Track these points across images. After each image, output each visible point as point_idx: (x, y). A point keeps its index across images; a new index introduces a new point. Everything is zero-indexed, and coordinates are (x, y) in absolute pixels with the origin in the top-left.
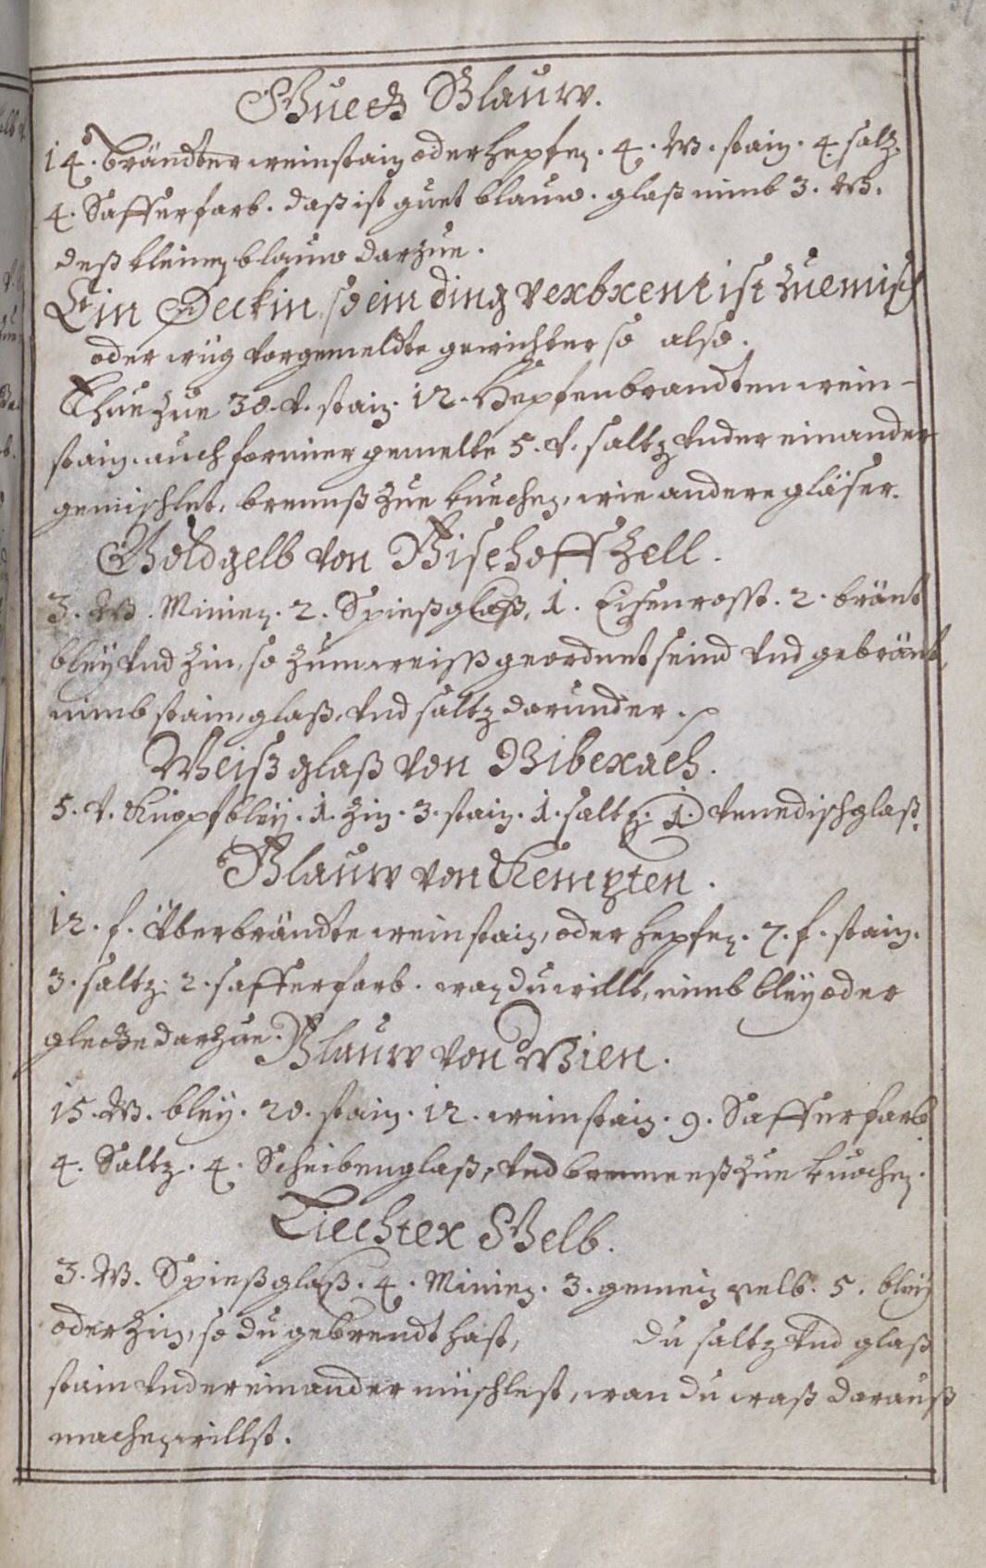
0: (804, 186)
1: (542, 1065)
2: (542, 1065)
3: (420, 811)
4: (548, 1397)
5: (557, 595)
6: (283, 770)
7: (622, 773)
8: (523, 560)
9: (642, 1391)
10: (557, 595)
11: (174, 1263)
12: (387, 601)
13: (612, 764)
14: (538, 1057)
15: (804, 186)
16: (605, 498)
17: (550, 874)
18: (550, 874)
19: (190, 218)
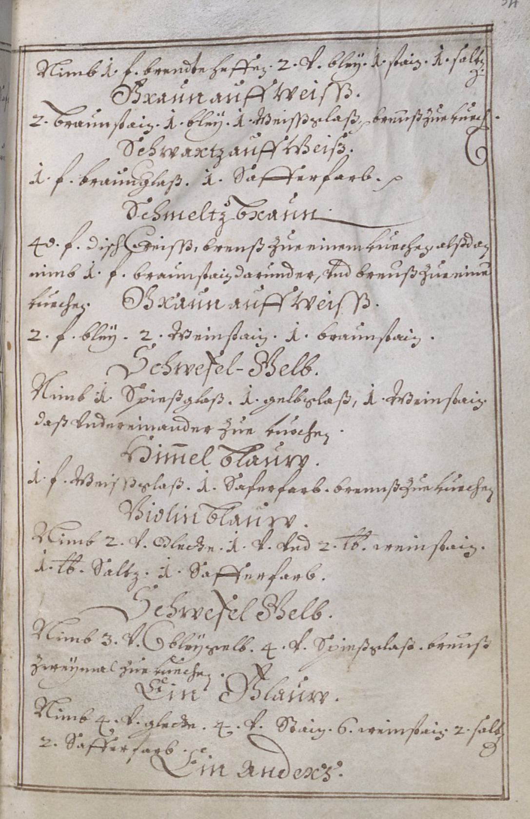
0: (344, 147)
1: (308, 307)
2: (308, 307)
3: (106, 639)
4: (384, 340)
5: (295, 331)
6: (183, 399)
7: (312, 778)
8: (278, 370)
9: (167, 274)
10: (295, 331)
11: (132, 389)
12: (255, 570)
13: (307, 774)
14: (305, 303)
15: (344, 147)
16: (259, 275)
17: (327, 302)
18: (327, 302)
19: (275, 492)
